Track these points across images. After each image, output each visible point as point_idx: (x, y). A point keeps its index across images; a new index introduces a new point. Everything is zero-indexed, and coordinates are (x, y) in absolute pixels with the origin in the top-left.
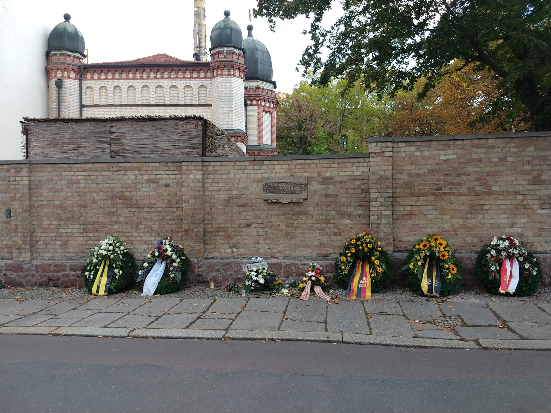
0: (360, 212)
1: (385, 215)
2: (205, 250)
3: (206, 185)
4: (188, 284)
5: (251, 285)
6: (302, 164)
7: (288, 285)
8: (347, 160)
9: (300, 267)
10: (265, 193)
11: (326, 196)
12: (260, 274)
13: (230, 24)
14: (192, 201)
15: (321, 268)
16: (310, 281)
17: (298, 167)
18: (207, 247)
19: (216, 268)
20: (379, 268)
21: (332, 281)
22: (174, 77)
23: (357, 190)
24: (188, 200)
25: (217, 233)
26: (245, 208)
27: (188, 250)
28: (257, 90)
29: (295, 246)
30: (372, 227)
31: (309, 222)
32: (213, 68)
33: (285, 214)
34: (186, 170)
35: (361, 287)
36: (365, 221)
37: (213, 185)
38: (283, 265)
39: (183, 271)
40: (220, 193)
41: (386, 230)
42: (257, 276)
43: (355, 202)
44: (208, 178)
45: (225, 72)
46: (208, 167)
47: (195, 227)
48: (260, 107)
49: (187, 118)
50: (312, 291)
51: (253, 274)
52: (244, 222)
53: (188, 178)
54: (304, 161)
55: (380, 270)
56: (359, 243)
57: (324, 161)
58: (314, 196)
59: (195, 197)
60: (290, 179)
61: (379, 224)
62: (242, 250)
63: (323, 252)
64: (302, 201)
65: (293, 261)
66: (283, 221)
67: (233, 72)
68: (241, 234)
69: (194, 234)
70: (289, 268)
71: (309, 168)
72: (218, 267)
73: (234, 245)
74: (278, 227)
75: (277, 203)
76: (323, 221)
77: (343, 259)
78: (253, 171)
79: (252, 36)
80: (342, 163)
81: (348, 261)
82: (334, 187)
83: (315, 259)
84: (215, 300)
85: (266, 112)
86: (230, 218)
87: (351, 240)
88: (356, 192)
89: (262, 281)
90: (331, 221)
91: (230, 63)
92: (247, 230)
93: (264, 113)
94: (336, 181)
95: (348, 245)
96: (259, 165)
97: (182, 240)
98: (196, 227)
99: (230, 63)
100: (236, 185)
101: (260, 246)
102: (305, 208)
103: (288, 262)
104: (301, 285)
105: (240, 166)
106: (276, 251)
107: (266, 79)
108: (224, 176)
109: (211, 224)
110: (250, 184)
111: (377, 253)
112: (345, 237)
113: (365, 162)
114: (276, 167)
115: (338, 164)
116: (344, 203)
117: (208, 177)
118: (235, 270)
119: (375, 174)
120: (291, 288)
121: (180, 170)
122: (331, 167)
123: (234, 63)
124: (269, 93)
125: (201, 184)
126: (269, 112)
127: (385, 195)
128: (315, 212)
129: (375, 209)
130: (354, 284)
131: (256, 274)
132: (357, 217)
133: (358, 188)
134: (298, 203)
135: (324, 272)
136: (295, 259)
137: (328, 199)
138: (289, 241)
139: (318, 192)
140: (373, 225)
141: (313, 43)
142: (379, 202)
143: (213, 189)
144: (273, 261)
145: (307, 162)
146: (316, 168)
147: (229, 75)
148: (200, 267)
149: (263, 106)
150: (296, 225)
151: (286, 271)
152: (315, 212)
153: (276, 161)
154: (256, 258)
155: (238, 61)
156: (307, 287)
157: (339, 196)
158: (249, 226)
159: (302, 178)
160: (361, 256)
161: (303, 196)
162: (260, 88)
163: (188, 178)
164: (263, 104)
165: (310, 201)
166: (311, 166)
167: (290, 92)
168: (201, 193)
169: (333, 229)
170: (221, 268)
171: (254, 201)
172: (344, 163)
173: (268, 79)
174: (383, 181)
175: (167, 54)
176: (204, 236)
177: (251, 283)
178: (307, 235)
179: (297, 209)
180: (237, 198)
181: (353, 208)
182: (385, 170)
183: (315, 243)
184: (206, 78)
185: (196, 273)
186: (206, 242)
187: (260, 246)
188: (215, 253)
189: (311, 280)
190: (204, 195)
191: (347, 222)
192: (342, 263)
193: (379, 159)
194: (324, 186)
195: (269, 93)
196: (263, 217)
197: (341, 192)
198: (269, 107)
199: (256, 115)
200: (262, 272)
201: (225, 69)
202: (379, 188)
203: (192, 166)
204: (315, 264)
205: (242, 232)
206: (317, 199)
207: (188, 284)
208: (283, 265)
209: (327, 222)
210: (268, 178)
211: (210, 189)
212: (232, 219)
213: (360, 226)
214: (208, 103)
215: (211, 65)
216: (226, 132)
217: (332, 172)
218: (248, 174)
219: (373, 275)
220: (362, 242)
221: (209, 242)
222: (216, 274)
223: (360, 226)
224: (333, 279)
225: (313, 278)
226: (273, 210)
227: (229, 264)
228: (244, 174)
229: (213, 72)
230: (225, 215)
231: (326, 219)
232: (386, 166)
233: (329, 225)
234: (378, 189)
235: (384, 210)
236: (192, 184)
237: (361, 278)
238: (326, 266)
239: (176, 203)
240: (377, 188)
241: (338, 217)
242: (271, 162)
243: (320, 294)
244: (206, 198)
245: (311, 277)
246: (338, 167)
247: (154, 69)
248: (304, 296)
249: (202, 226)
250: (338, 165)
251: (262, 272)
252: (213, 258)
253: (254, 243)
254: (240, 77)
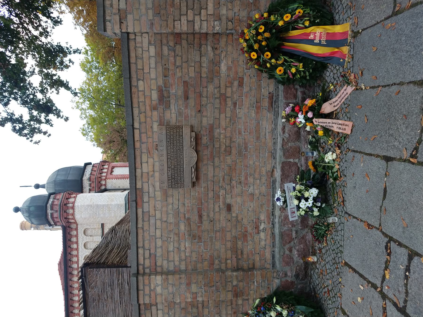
0: (209, 48)
1: (215, 9)
2: (262, 268)
3: (172, 268)
4: (308, 289)
5: (320, 209)
6: (140, 133)
7: (315, 153)
8: (133, 67)
9: (287, 135)
10: (182, 186)
11: (187, 98)
12: (303, 195)
13: (25, 207)
14: (194, 289)
15: (291, 105)
16: (314, 120)
17: (144, 139)
18: (258, 264)
19: (287, 252)
20: (297, 13)
21: (308, 90)
22: (76, 259)
23: (177, 52)
24: (193, 293)
25: (239, 252)
26: (204, 213)
27: (262, 292)
28: (92, 180)
29: (257, 144)
30: (231, 30)
31: (223, 124)
32: (67, 223)
33: (212, 158)
34: (150, 297)
35: (326, 41)
36: (223, 41)
37: (171, 259)
38: (283, 159)
39: (294, 302)
40: (183, 249)
41: (236, 8)
42: (307, 199)
43: (195, 56)
44: (161, 266)
45: (71, 211)
46: (146, 266)
47: (230, 283)
48: (108, 177)
49: (83, 287)
50: (329, 116)
51: (303, 205)
52: (224, 213)
53: (162, 295)
54: (135, 130)
55: (299, 12)
56: (256, 47)
57: (135, 101)
58: (186, 117)
59: (189, 284)
60: (161, 151)
61: (227, 18)
62: (263, 217)
63: (266, 103)
64: (194, 134)
65: (279, 145)
66: (222, 159)
67: (70, 205)
68: (239, 218)
69: (241, 284)
70: (288, 151)
71: (145, 122)
72: (286, 249)
73: (256, 228)
74: (230, 167)
75: (197, 169)
76: (223, 103)
77: (279, 71)
78: (152, 203)
79: (44, 185)
80: (137, 75)
81: (283, 63)
82: (174, 87)
83: (277, 114)
84: (346, 264)
85: (112, 172)
86: (218, 234)
87: (251, 60)
88: (180, 54)
89: (314, 192)
90: (223, 91)
91: (62, 208)
92: (235, 210)
93: (113, 173)
94: (165, 84)
95: (259, 65)
96: (143, 195)
97: (248, 300)
98: (231, 282)
99: (62, 208)
100: (172, 227)
101: (257, 192)
102: (204, 129)
103: (279, 153)
104: (321, 133)
105: (143, 221)
106: (264, 169)
107: (82, 171)
108: (159, 243)
109: (226, 259)
110: (171, 206)
111: (272, 18)
112: (246, 71)
113: (135, 39)
114: (145, 170)
115: (138, 80)
116: (197, 72)
117: (159, 266)
118: (290, 226)
119: (152, 24)
120: (320, 149)
121: (151, 305)
122: (144, 91)
123: (62, 203)
124: (95, 169)
125: (170, 277)
126: (112, 169)
127: (184, 9)
128: (209, 114)
129: (205, 24)
130: (320, 52)
131: (303, 201)
132: (217, 52)
133: (175, 51)
134: (197, 139)
135: (294, 101)
136: (275, 143)
137: (191, 95)
138: (250, 152)
139: (181, 111)
140: (229, 28)
141: (9, 125)
142: (194, 18)
143: (177, 259)
144: (278, 174)
145: (136, 125)
146: (145, 112)
147: (73, 208)
148: (286, 275)
149: (107, 174)
150: (228, 141)
151: (292, 155)
152: (209, 114)
153: (137, 170)
154: (278, 199)
155: (60, 200)
156: (324, 125)
157: (187, 79)
158: (229, 208)
159: (161, 134)
160: (278, 42)
161: (186, 132)
162: (90, 177)
163: (161, 295)
164: (105, 174)
165: (194, 121)
166: (143, 120)
167: (100, 150)
168: (183, 276)
169: (234, 89)
170: (287, 246)
171: (194, 201)
172: (136, 72)
173: (82, 170)
174: (162, 12)
175: (58, 262)
176: (242, 269)
177: (317, 207)
178: (242, 127)
179: (205, 140)
180: (190, 224)
181: (204, 59)
182: (147, 9)
183: (254, 115)
184: (76, 229)
185: (294, 279)
186: (251, 266)
187: (257, 192)
188: (267, 254)
189: (312, 118)
190: (186, 270)
191: (223, 67)
192: (285, 73)
193: (130, 17)
194: (171, 101)
195: (95, 169)
196: (216, 188)
197: (181, 77)
198: (108, 169)
199: (114, 181)
200: (300, 191)
201: (68, 211)
202: (174, 16)
203: (144, 290)
204: (284, 114)
205: (237, 217)
206: (190, 112)
207: (308, 289)
208: (283, 159)
209: (223, 98)
210: (161, 182)
211: (177, 263)
212: (219, 231)
213: (230, 48)
214: (100, 227)
215: (64, 225)
216: (128, 212)
217: (151, 90)
218: (155, 210)
219: (307, 23)
220: (255, 42)
221: (251, 262)
222: (295, 252)
223: (230, 48)
224: (305, 88)
225: (310, 115)
226: (206, 175)
227: (282, 235)
228: (155, 216)
229: (71, 222)
230: (214, 240)
231: (219, 98)
232: (141, 7)
233: (229, 94)
234: (176, 19)
235: (207, 11)
236: (170, 288)
237: (311, 42)
238: (286, 98)
239: (198, 308)
240: (174, 21)
241: (216, 81)
242: (138, 179)
243: (336, 104)
244: (190, 267)
245: (307, 119)
246: (143, 80)
247: (70, 277)
248: (340, 128)
249: (229, 273)
250: (139, 80)
251: (300, 191)
252: (273, 257)
253: (252, 200)
254: (75, 198)
